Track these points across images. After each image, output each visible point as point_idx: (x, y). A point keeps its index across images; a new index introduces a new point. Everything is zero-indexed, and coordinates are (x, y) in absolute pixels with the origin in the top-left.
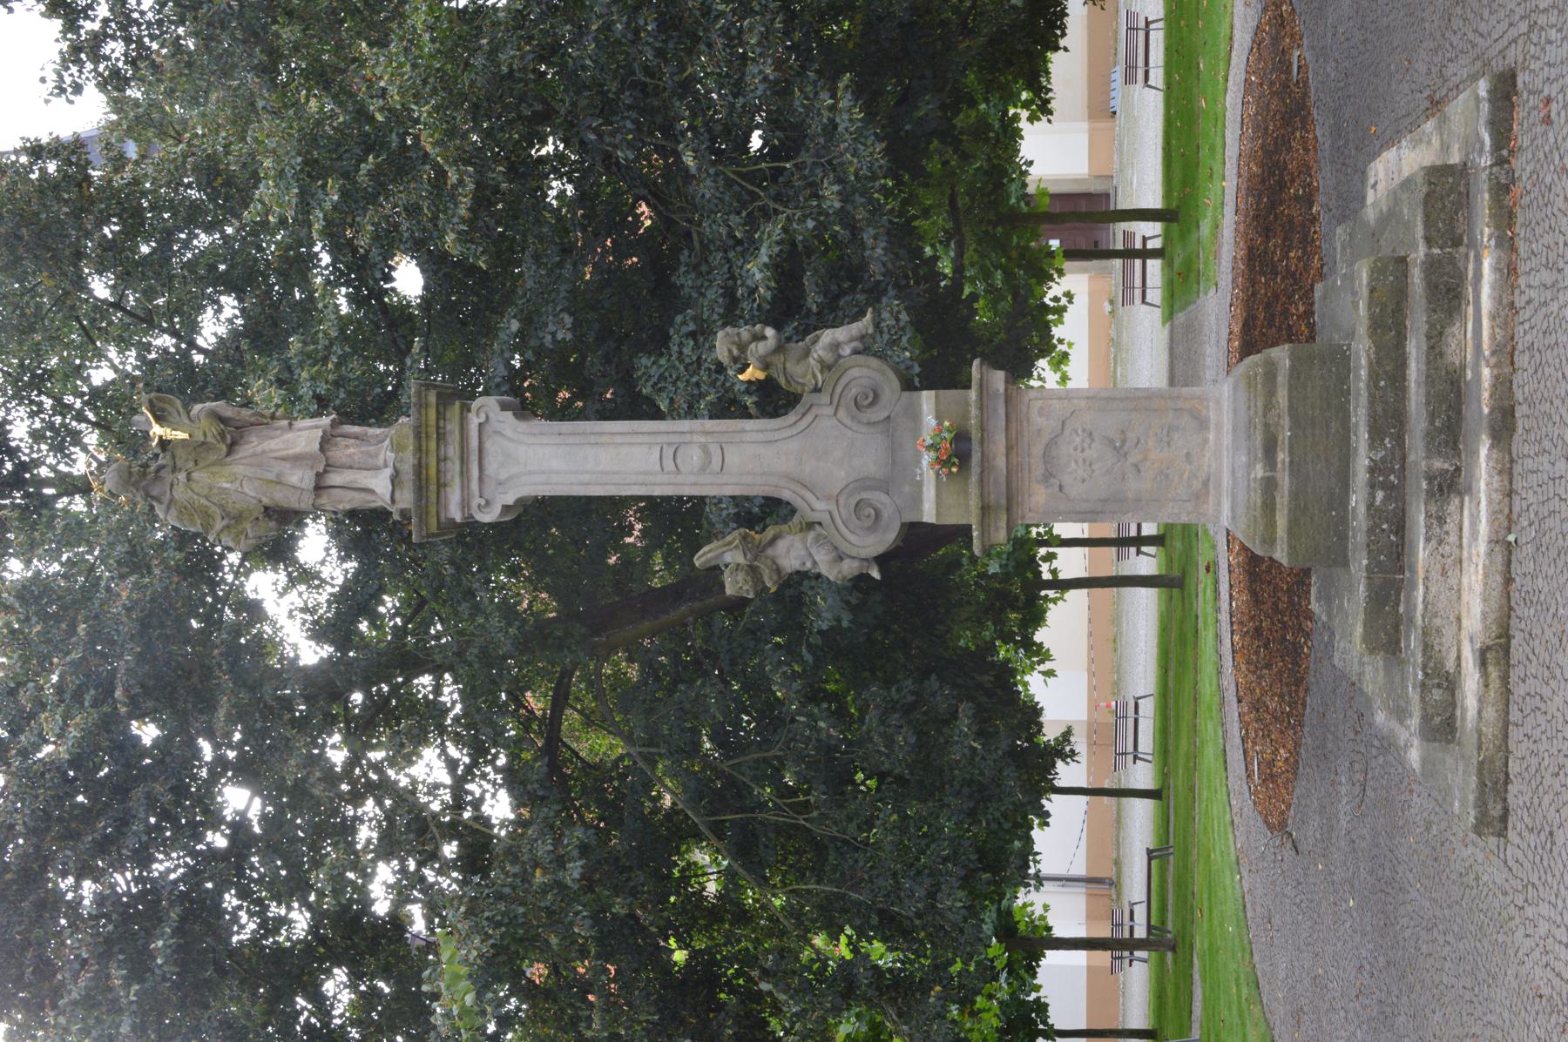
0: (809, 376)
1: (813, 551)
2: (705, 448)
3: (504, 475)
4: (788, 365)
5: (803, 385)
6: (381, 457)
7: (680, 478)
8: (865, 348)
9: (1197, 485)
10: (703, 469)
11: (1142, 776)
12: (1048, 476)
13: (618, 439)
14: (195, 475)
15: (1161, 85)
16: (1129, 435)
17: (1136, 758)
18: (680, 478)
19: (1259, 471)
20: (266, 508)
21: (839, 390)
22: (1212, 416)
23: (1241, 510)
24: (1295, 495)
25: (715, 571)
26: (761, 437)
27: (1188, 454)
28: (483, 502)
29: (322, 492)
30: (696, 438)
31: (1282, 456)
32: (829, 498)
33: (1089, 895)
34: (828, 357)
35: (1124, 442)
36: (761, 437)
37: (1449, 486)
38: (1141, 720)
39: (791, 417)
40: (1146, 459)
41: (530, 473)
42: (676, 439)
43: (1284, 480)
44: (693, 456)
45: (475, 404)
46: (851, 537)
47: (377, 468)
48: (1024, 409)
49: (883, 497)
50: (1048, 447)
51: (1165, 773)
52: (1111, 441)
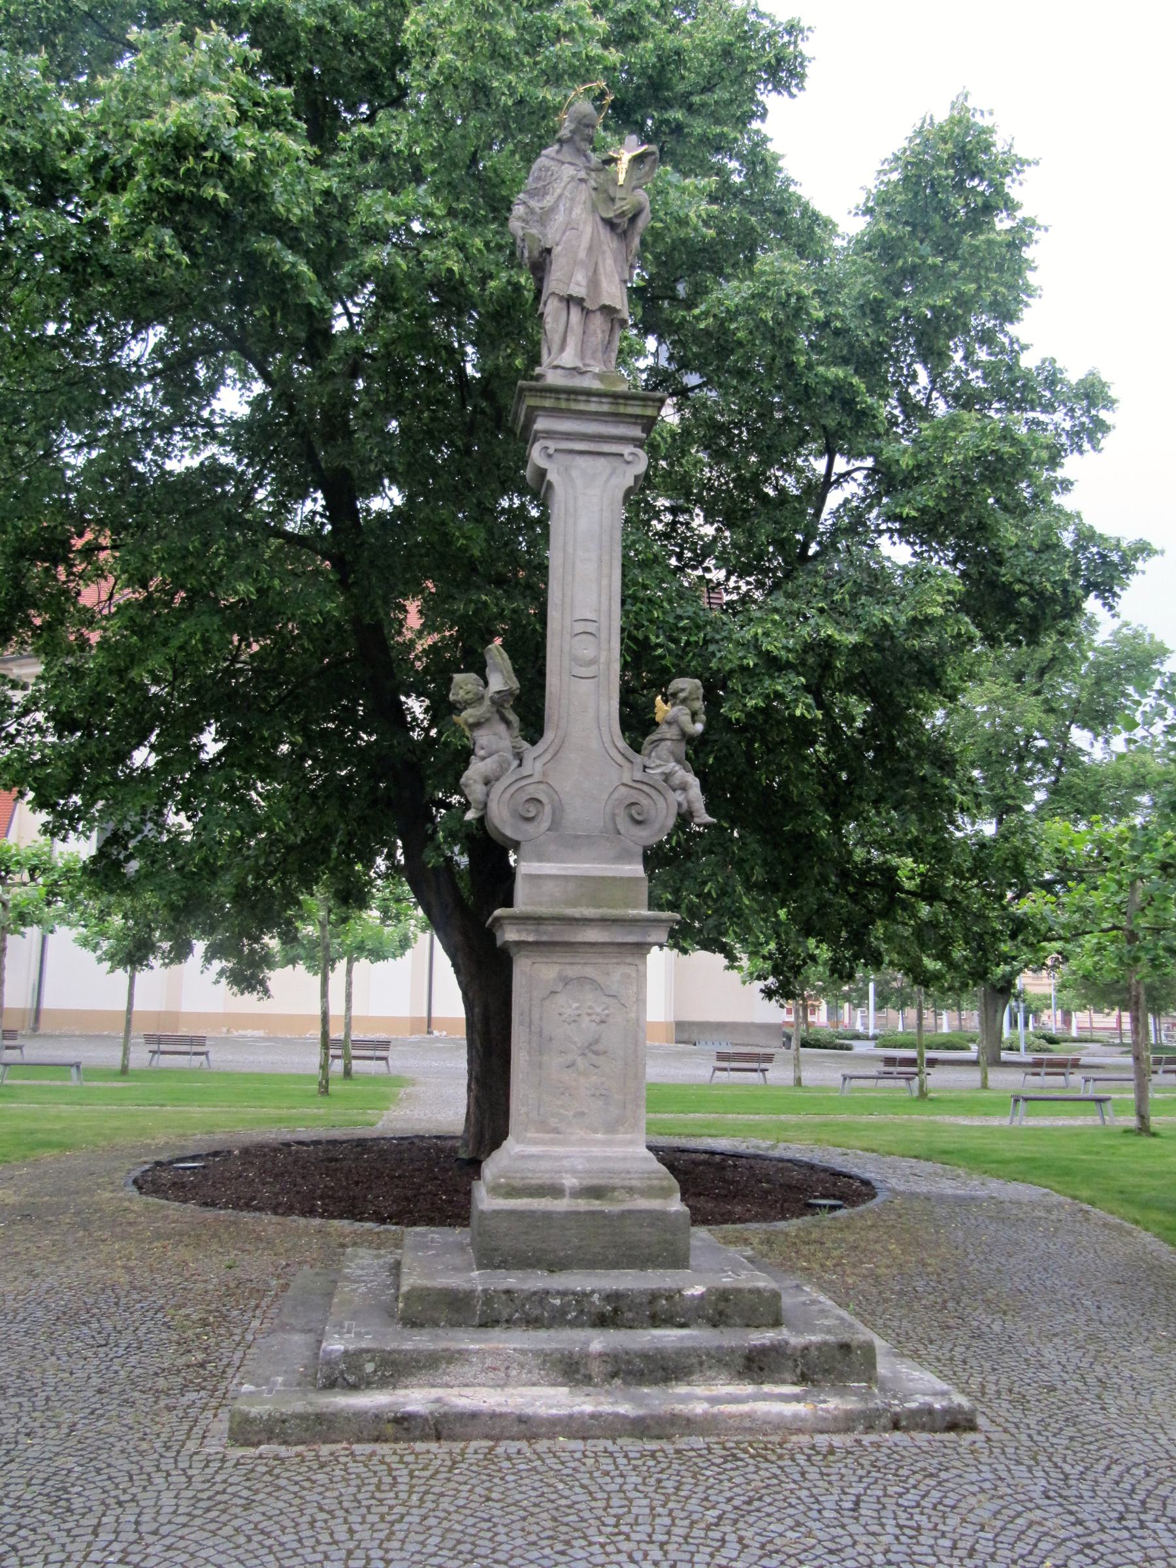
0: (658, 762)
1: (495, 757)
2: (593, 662)
3: (575, 473)
4: (669, 743)
5: (649, 756)
6: (592, 362)
7: (567, 637)
8: (685, 818)
9: (553, 1122)
10: (575, 659)
11: (140, 1056)
12: (566, 981)
13: (605, 582)
14: (584, 186)
15: (715, 1081)
16: (602, 1058)
17: (154, 1052)
18: (567, 637)
19: (569, 1182)
20: (549, 251)
21: (645, 788)
22: (620, 1137)
23: (531, 1165)
24: (547, 1215)
25: (479, 667)
26: (603, 715)
27: (583, 1114)
28: (551, 451)
29: (564, 305)
30: (604, 654)
31: (583, 1205)
32: (544, 774)
33: (24, 1011)
34: (676, 780)
35: (596, 1053)
36: (603, 715)
37: (571, 1370)
38: (187, 1057)
39: (622, 744)
40: (580, 1074)
41: (575, 498)
42: (604, 635)
43: (562, 1205)
44: (586, 649)
45: (642, 454)
46: (507, 795)
47: (582, 357)
48: (629, 960)
49: (545, 825)
50: (592, 981)
51: (140, 1075)
52: (597, 1041)
